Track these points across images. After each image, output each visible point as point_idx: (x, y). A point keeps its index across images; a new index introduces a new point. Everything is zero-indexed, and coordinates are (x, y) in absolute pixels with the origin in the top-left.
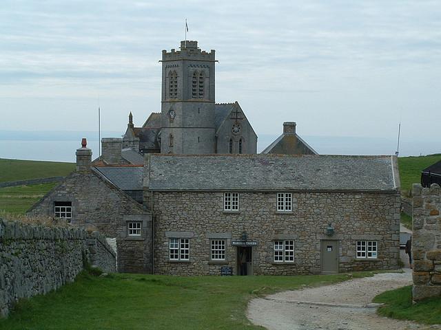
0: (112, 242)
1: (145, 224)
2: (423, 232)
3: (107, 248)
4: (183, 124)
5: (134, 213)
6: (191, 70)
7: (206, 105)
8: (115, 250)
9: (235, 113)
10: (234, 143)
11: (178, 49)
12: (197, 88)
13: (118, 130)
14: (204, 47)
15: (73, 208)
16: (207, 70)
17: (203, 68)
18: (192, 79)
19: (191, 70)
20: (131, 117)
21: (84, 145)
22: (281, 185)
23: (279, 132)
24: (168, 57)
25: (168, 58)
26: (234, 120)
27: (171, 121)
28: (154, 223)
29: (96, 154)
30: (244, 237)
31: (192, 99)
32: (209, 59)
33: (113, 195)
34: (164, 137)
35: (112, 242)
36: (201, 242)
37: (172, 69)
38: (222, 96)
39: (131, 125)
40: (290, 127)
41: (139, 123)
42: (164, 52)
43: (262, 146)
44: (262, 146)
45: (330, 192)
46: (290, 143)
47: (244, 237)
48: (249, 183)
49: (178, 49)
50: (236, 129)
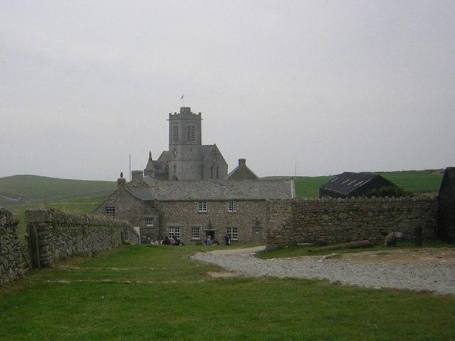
0: (137, 229)
1: (155, 219)
2: (271, 221)
3: (134, 233)
5: (150, 213)
8: (139, 233)
9: (214, 151)
11: (178, 112)
13: (141, 166)
14: (194, 111)
15: (233, 224)
16: (196, 125)
18: (187, 131)
20: (150, 154)
21: (122, 175)
22: (230, 197)
23: (236, 165)
24: (172, 118)
25: (172, 118)
27: (175, 156)
28: (161, 218)
29: (128, 178)
30: (210, 226)
32: (198, 118)
33: (137, 203)
34: (171, 165)
35: (137, 229)
37: (175, 125)
38: (206, 141)
39: (150, 159)
40: (242, 162)
41: (155, 158)
42: (170, 114)
43: (230, 170)
44: (230, 170)
45: (254, 200)
46: (243, 171)
47: (210, 226)
48: (213, 196)
49: (178, 112)
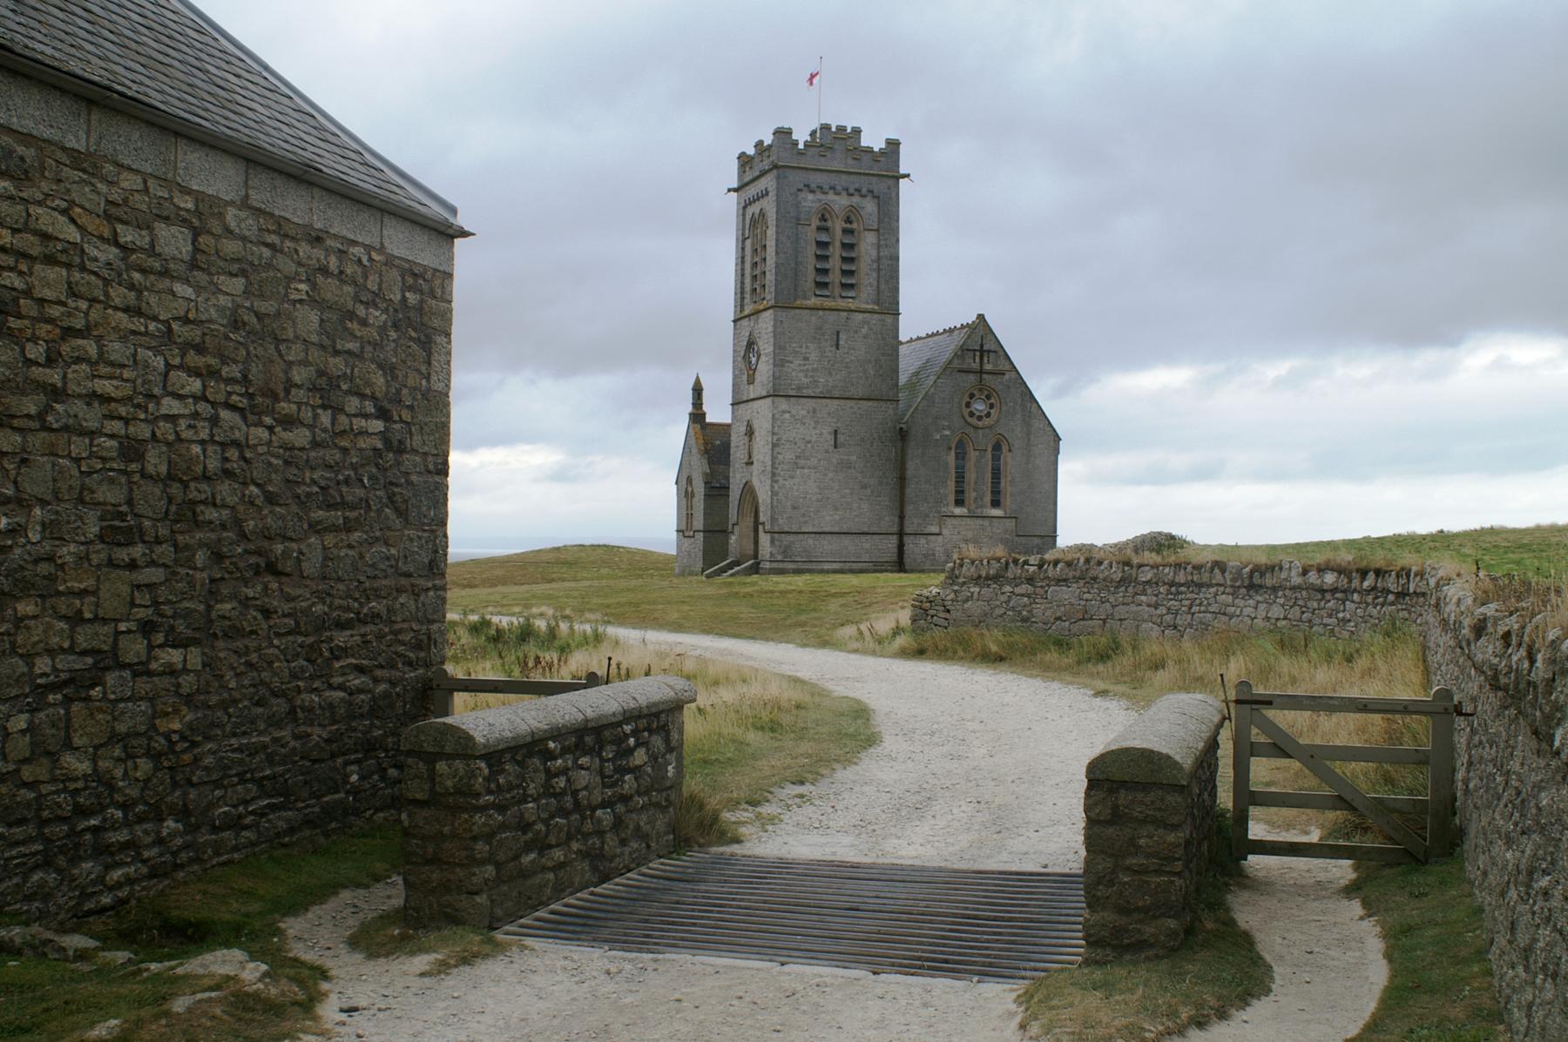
4: (774, 390)
6: (810, 201)
7: (864, 322)
10: (973, 455)
12: (835, 264)
14: (873, 140)
16: (869, 206)
17: (856, 199)
19: (810, 201)
26: (972, 377)
31: (813, 301)
36: (29, 590)
50: (979, 406)
